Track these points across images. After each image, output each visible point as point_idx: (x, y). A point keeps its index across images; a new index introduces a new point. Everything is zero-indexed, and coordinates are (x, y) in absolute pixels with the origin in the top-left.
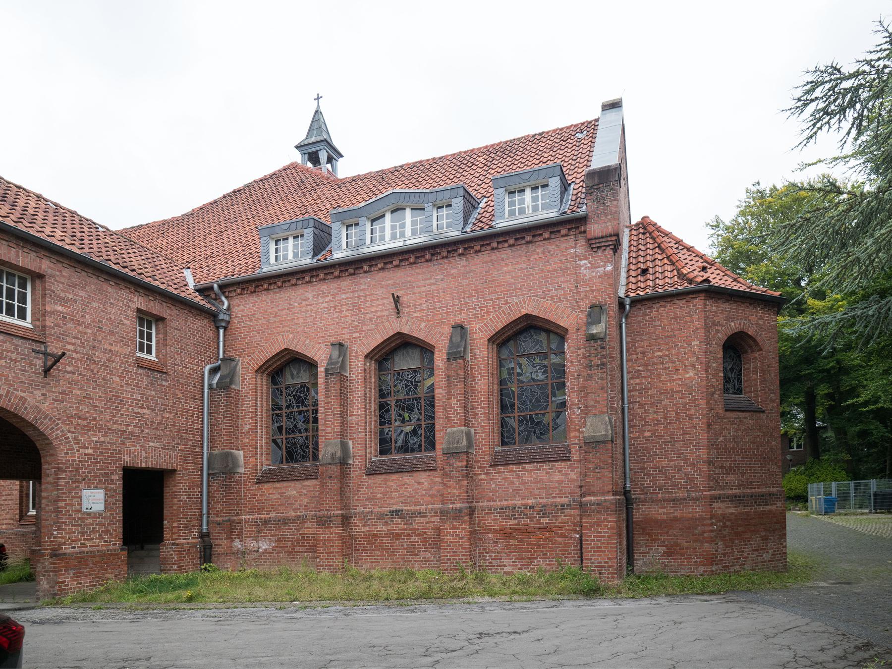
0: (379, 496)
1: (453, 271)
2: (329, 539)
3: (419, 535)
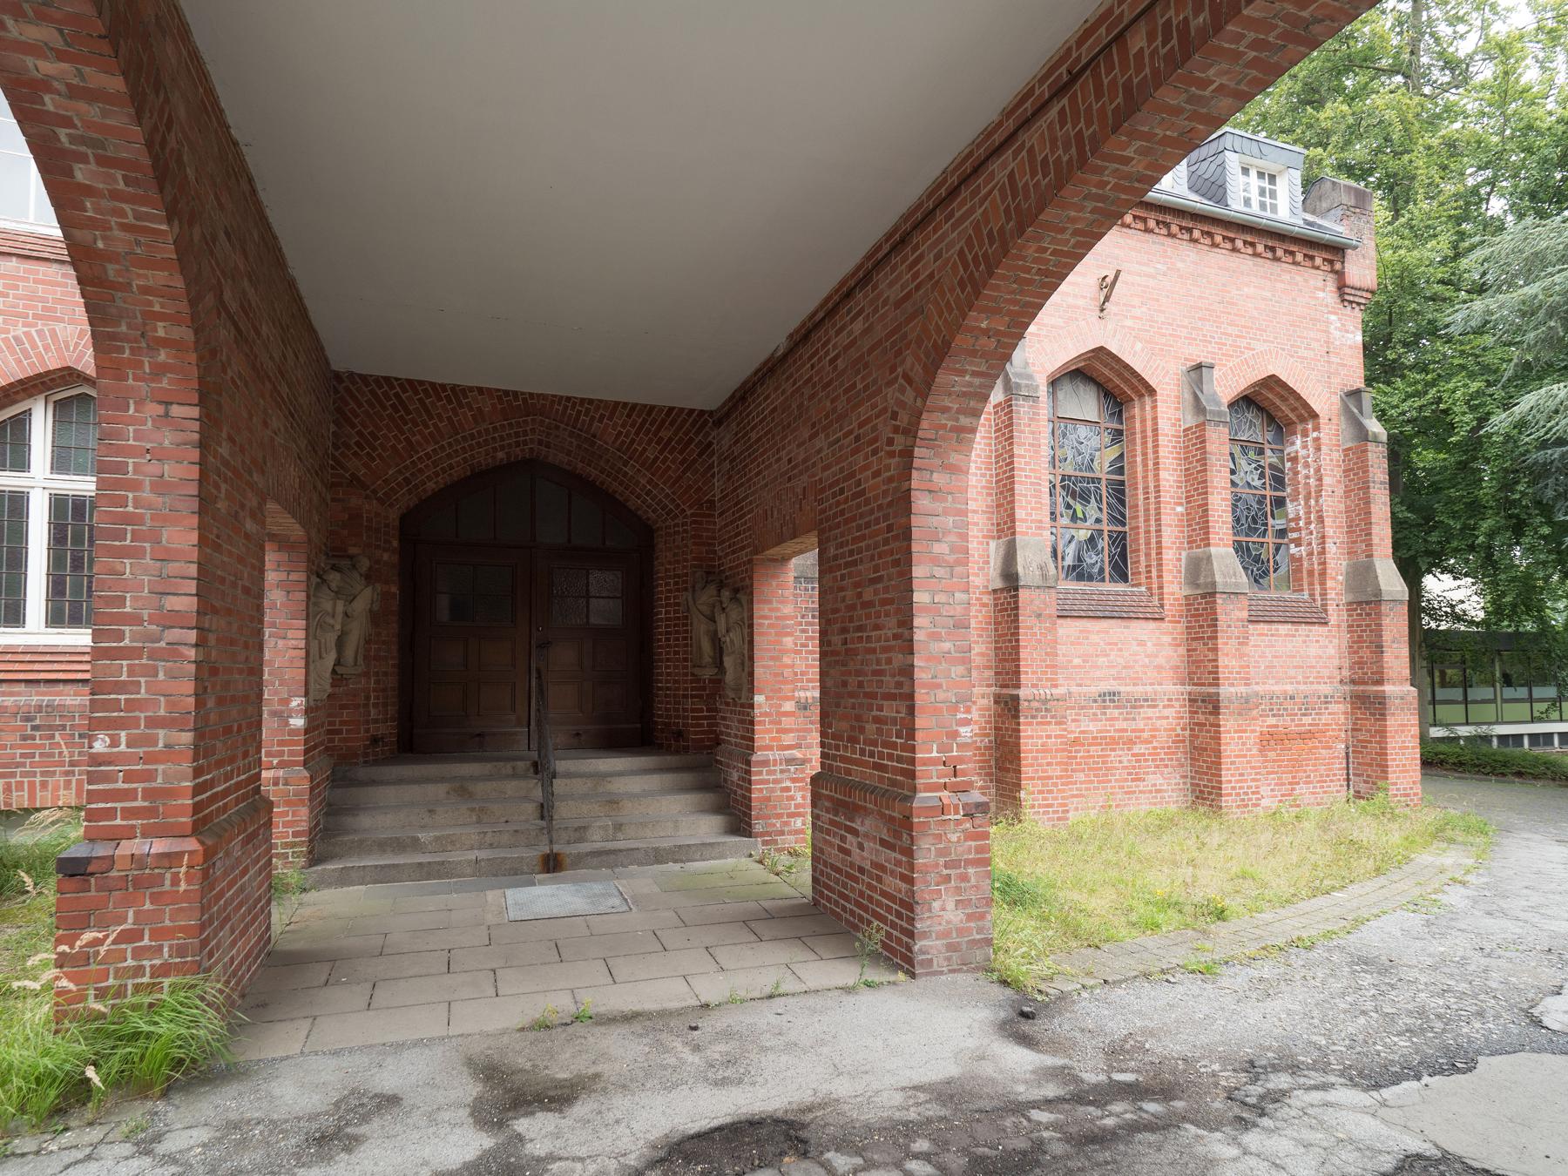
0: (1077, 661)
1: (1180, 265)
2: (1045, 750)
3: (1147, 742)
